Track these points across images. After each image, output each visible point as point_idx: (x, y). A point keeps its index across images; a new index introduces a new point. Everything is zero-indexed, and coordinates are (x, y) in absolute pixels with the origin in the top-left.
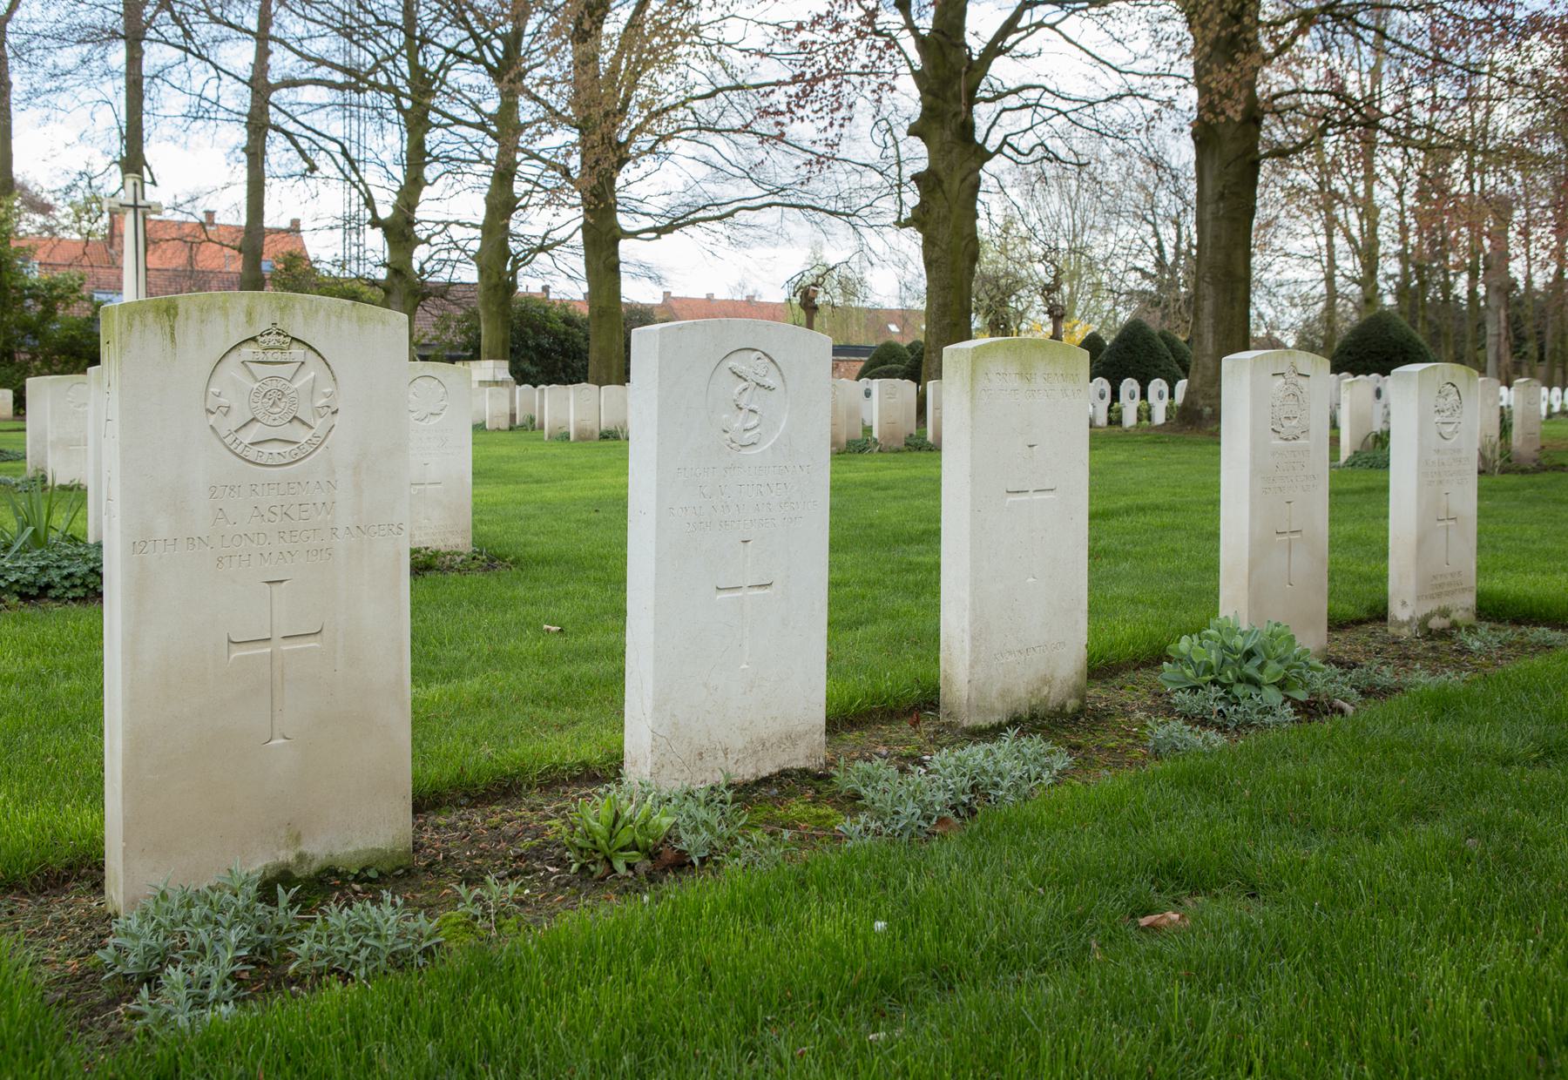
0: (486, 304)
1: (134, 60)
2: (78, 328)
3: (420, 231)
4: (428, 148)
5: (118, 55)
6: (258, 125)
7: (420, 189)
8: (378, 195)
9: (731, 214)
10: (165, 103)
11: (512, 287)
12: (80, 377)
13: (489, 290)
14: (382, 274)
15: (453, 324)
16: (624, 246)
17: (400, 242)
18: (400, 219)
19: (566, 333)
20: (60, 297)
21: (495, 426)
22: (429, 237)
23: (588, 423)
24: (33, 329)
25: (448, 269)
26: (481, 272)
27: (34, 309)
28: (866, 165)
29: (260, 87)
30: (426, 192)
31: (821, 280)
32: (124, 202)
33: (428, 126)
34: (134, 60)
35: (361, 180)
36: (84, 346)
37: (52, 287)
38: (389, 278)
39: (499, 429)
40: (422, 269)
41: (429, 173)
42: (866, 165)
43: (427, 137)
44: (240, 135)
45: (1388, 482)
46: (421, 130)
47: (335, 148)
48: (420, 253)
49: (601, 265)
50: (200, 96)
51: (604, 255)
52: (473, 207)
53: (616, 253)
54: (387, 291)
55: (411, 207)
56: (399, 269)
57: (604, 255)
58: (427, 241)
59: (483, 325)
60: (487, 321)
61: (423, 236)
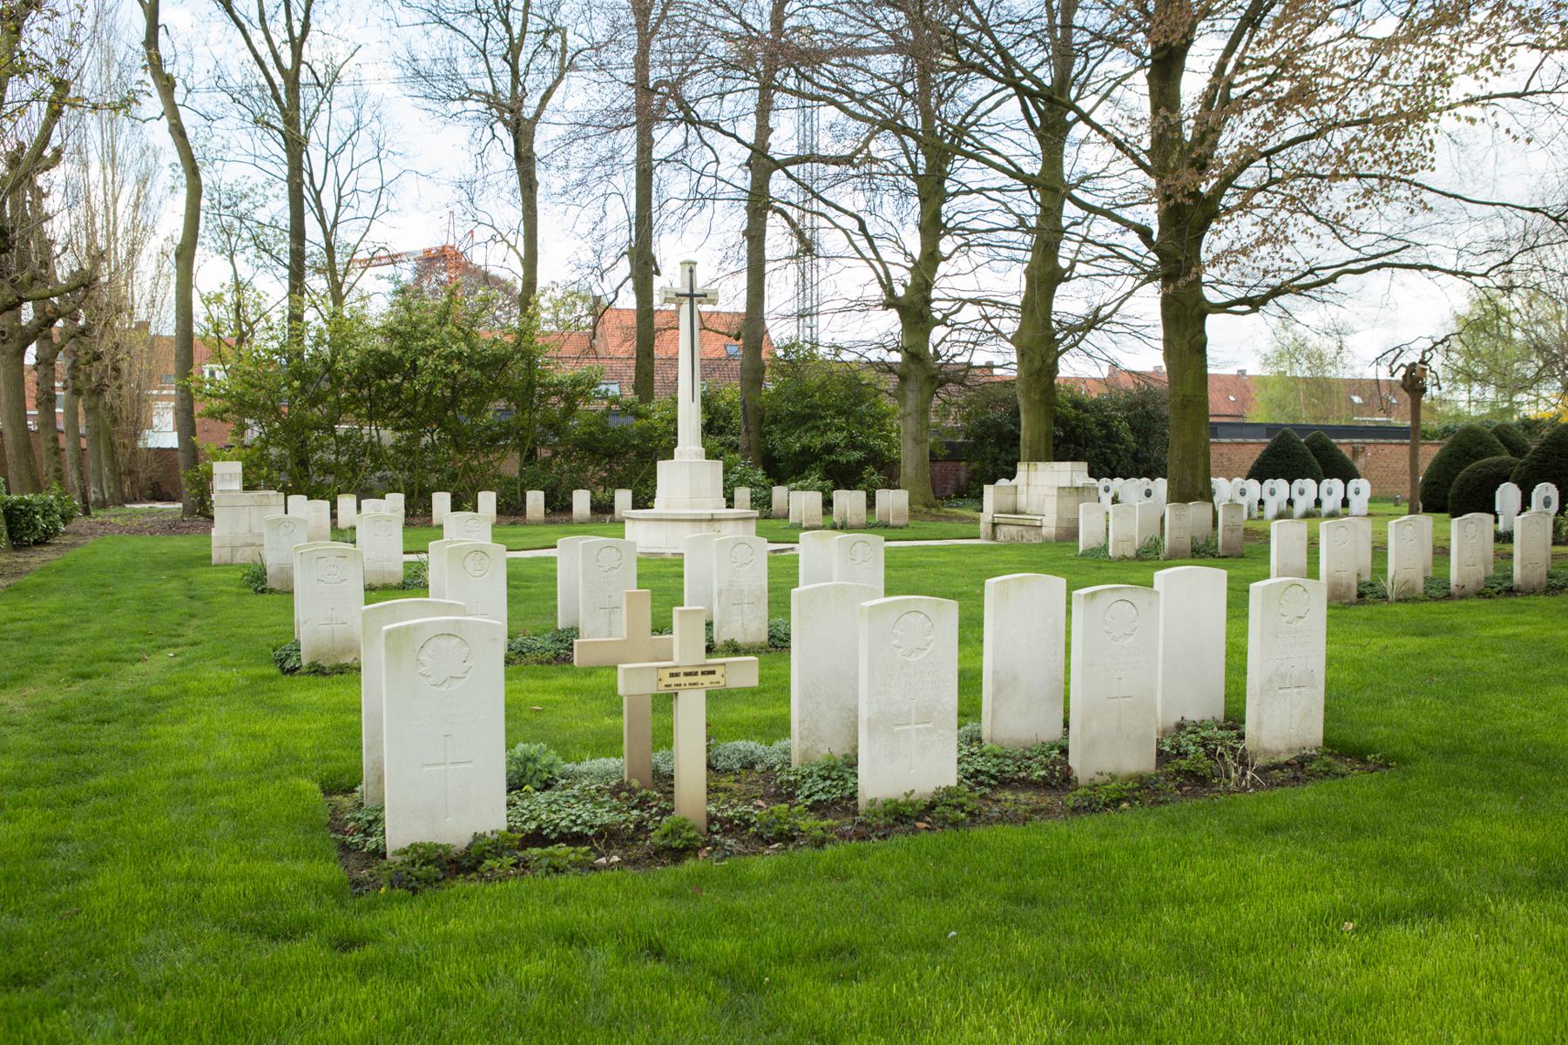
0: (1027, 392)
1: (645, 146)
2: (596, 423)
3: (938, 308)
4: (944, 220)
5: (628, 137)
6: (759, 204)
7: (937, 264)
8: (896, 272)
9: (1333, 279)
10: (672, 184)
11: (1053, 370)
12: (1138, 595)
13: (1031, 375)
14: (896, 357)
15: (953, 410)
16: (1213, 322)
17: (916, 323)
18: (916, 298)
19: (1077, 418)
20: (582, 393)
21: (1119, 554)
22: (946, 317)
23: (1344, 575)
24: (554, 427)
25: (967, 354)
26: (1022, 355)
27: (557, 404)
28: (1534, 210)
29: (761, 162)
30: (943, 268)
31: (1428, 355)
32: (680, 292)
33: (943, 196)
34: (645, 146)
35: (879, 258)
36: (599, 441)
37: (576, 383)
38: (904, 364)
39: (1125, 557)
40: (936, 351)
41: (946, 245)
42: (1534, 210)
43: (944, 207)
44: (739, 218)
45: (676, 415)
46: (937, 200)
47: (852, 224)
48: (937, 333)
49: (1186, 346)
50: (716, 177)
51: (1188, 334)
52: (1011, 282)
53: (1202, 331)
54: (903, 378)
55: (929, 286)
56: (916, 355)
57: (1188, 334)
58: (943, 322)
59: (1022, 415)
60: (1027, 412)
61: (938, 316)
